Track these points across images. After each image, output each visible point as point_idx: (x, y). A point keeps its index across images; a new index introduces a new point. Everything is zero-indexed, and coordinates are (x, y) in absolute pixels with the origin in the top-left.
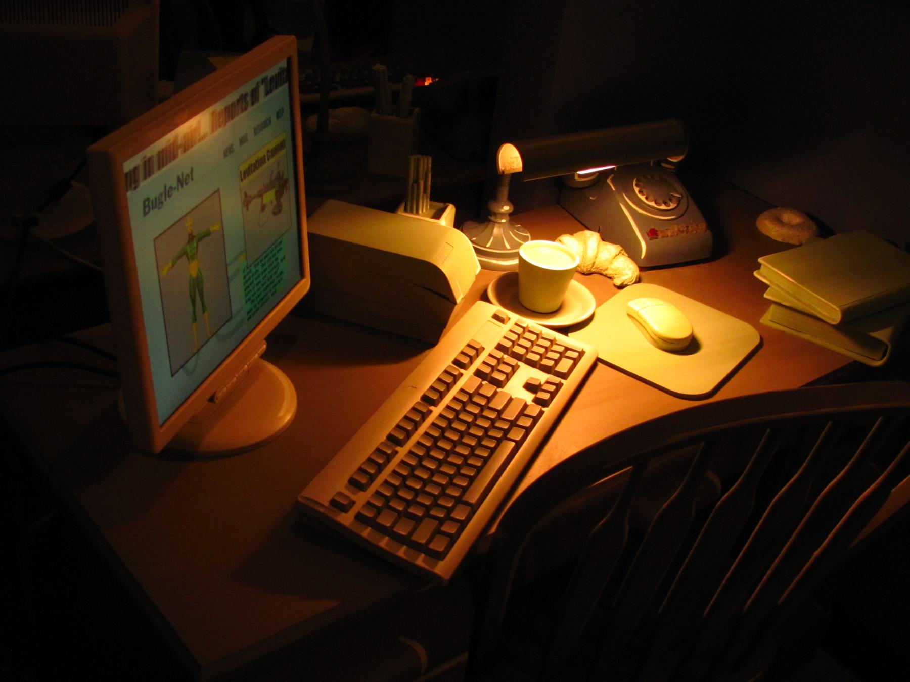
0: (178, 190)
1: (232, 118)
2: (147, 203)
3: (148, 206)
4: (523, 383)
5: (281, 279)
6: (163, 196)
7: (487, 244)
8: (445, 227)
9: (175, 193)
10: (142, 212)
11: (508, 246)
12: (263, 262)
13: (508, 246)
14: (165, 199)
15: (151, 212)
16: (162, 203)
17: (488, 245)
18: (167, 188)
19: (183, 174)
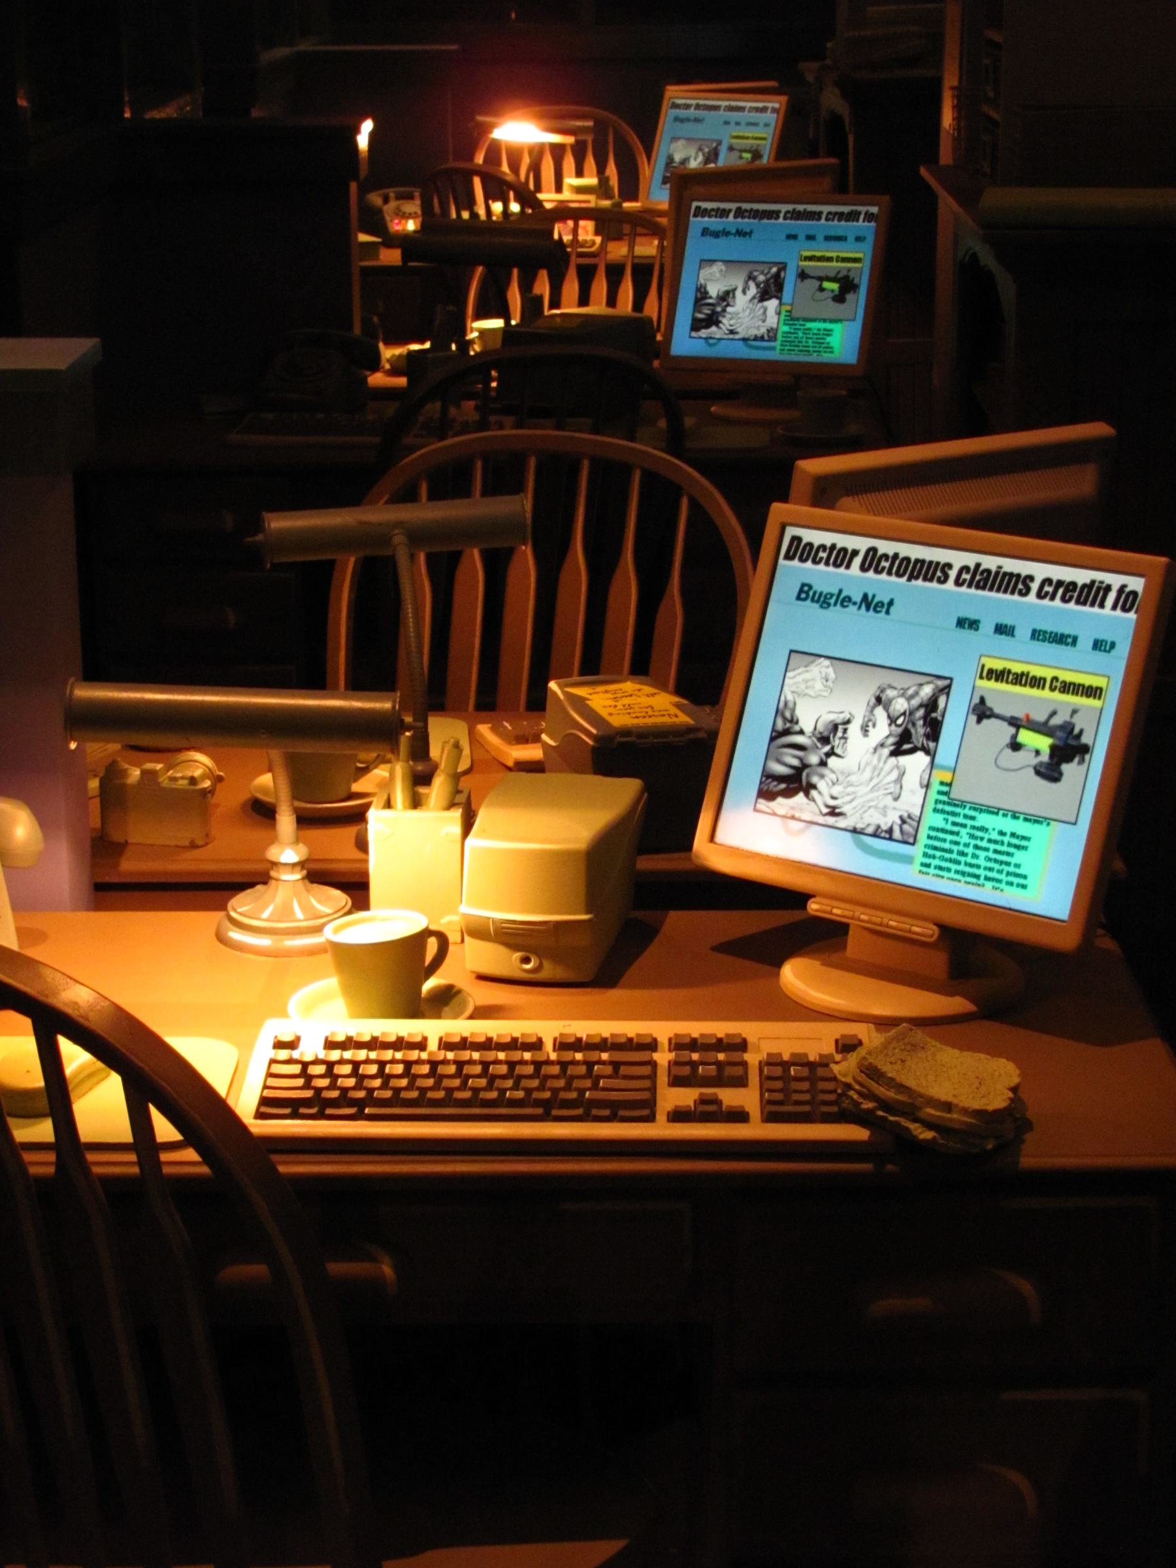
0: (860, 608)
1: (815, 504)
2: (806, 588)
3: (807, 593)
4: (866, 739)
5: (862, 506)
6: (834, 598)
7: (263, 912)
8: (132, 766)
9: (852, 609)
10: (795, 594)
11: (299, 914)
12: (966, 850)
13: (299, 914)
14: (835, 604)
15: (808, 602)
16: (829, 605)
17: (266, 915)
18: (842, 596)
19: (874, 596)
